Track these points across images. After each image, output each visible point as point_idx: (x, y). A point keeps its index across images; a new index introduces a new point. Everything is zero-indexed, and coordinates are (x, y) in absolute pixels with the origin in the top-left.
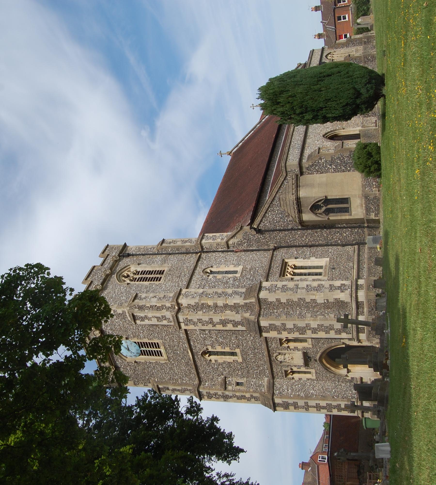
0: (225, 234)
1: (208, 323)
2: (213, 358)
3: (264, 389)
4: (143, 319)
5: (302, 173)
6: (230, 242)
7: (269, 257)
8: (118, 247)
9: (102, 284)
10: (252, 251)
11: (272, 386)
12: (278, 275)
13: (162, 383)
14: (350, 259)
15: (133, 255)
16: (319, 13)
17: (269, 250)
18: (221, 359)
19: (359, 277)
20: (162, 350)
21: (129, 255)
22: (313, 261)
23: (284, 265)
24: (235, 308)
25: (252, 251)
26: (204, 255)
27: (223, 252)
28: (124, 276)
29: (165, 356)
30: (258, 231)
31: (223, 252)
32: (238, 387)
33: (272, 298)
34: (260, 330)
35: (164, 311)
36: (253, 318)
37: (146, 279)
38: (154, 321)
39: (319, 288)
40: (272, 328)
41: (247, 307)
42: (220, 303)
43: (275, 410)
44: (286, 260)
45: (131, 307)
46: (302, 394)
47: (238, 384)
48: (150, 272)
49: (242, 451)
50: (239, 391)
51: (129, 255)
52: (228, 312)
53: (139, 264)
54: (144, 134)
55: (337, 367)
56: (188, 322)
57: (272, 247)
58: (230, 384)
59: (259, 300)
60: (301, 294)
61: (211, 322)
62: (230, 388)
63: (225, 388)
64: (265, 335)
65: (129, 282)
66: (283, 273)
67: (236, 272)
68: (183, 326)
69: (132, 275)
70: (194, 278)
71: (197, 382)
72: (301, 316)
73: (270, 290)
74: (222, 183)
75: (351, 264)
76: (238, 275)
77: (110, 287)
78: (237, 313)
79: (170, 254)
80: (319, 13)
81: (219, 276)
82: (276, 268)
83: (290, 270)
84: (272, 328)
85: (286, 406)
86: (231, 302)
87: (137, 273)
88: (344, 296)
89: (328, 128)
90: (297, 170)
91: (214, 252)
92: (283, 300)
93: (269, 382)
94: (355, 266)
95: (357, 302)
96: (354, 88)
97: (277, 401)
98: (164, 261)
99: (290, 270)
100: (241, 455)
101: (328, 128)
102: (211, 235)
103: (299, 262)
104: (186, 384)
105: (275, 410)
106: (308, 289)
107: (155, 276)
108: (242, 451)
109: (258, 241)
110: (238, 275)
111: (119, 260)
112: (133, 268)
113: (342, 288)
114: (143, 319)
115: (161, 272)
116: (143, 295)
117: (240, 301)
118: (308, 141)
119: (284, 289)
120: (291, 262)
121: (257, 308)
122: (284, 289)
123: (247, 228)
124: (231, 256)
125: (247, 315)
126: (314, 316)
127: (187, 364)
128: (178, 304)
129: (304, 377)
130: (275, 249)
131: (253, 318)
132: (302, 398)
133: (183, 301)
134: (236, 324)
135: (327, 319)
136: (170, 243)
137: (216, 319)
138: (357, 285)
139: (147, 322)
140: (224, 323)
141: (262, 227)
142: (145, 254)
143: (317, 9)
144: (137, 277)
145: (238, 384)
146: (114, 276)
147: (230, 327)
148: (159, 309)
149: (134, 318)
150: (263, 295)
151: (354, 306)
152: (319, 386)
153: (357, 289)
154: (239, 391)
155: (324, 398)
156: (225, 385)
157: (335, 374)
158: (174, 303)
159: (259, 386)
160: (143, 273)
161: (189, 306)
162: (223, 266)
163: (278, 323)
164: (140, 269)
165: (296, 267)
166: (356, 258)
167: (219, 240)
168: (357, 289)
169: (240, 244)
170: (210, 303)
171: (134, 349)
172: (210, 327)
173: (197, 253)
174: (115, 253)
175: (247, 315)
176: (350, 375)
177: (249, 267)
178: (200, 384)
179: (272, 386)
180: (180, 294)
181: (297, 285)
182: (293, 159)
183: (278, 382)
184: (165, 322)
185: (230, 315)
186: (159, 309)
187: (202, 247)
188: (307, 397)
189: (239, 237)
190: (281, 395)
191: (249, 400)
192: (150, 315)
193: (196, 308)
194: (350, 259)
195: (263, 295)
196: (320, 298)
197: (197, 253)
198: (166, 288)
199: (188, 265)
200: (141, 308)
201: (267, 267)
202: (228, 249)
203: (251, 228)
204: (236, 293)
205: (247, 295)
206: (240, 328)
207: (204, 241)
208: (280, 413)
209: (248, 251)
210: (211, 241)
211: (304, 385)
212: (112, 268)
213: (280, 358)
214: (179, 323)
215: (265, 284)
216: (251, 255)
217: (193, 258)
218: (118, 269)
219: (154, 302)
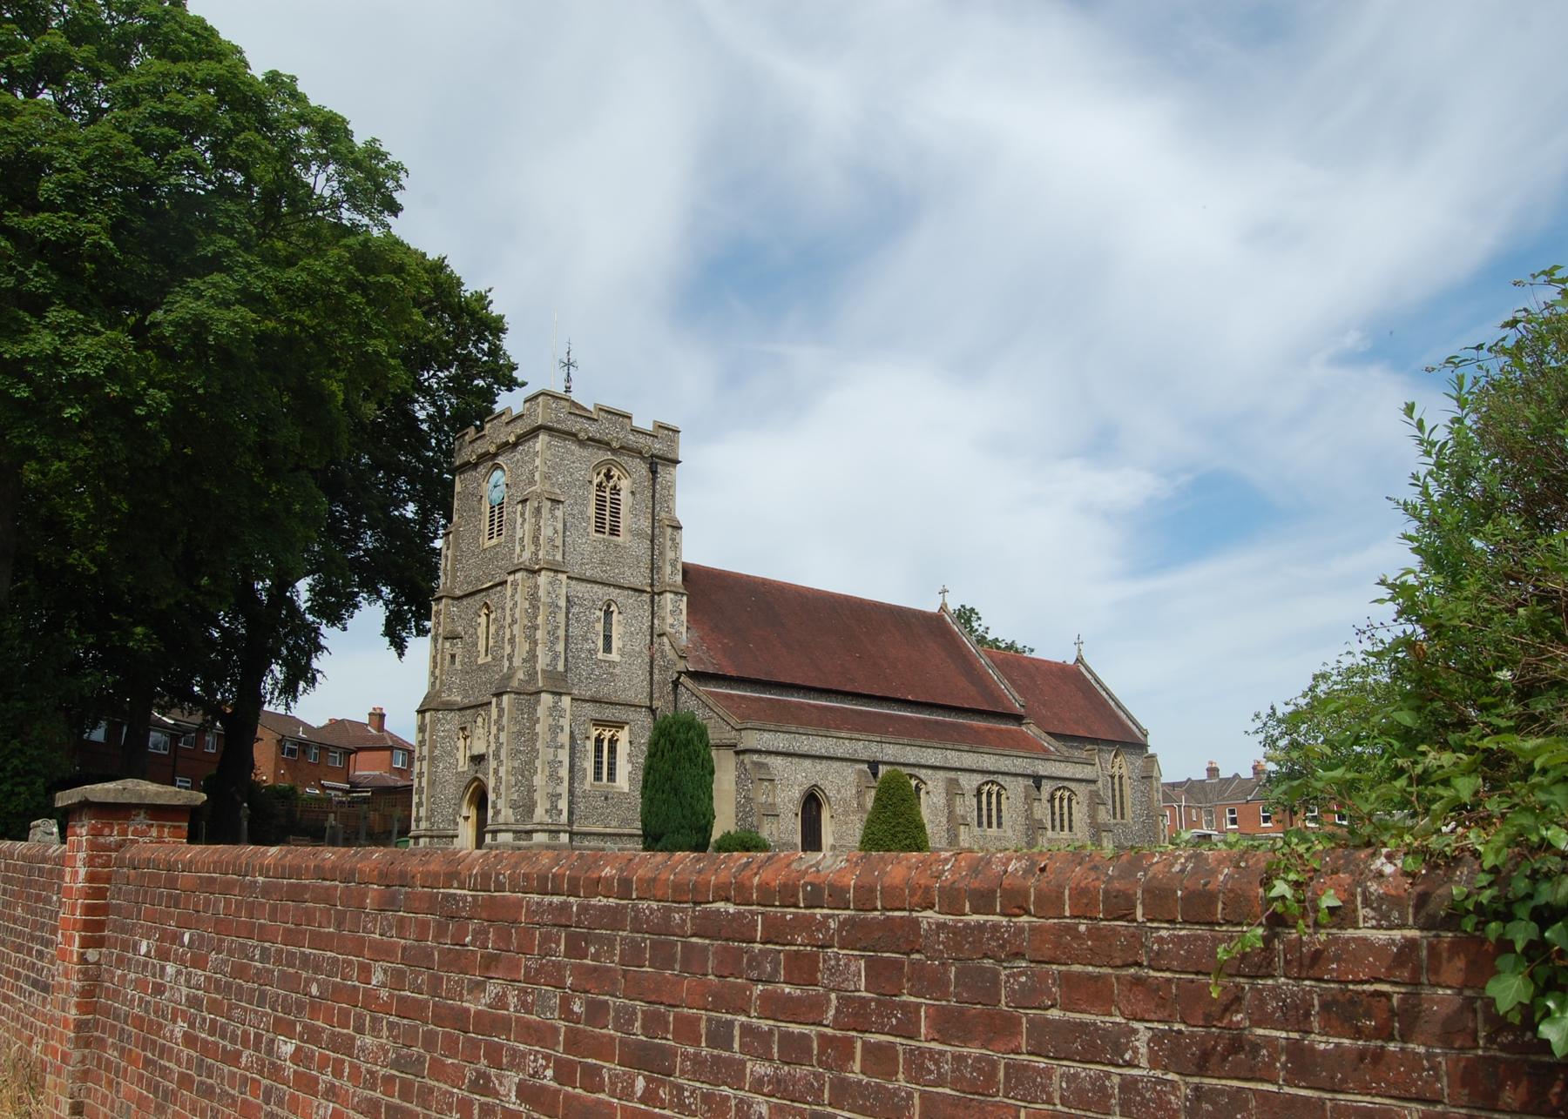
0: (684, 630)
1: (512, 616)
2: (483, 620)
3: (445, 697)
4: (522, 514)
5: (737, 753)
6: (665, 639)
7: (636, 702)
8: (674, 449)
9: (589, 439)
10: (651, 674)
11: (449, 707)
12: (597, 716)
13: (456, 539)
14: (625, 822)
15: (654, 479)
16: (1203, 776)
17: (651, 700)
18: (482, 631)
19: (515, 832)
20: (494, 541)
21: (654, 472)
22: (623, 768)
23: (619, 725)
24: (532, 657)
25: (651, 674)
26: (646, 597)
27: (652, 627)
28: (609, 471)
29: (488, 544)
30: (676, 684)
31: (652, 627)
32: (448, 657)
33: (541, 711)
34: (499, 695)
35: (533, 548)
36: (515, 683)
37: (600, 507)
38: (519, 534)
39: (554, 777)
40: (501, 710)
41: (532, 675)
42: (539, 634)
43: (419, 712)
44: (627, 728)
45: (539, 495)
46: (437, 752)
47: (453, 656)
48: (615, 513)
49: (401, 655)
50: (443, 659)
51: (654, 472)
52: (527, 647)
53: (633, 493)
54: (1351, 340)
55: (471, 802)
56: (515, 584)
57: (656, 704)
58: (453, 645)
59: (539, 693)
60: (545, 754)
61: (514, 622)
62: (447, 645)
63: (446, 638)
64: (494, 700)
65: (596, 482)
66: (598, 723)
67: (608, 648)
68: (510, 578)
69: (611, 484)
70: (596, 587)
71: (458, 593)
72: (514, 754)
73: (555, 707)
74: (862, 600)
75: (614, 824)
76: (600, 655)
77: (585, 453)
78: (524, 660)
79: (652, 541)
80: (1203, 776)
81: (599, 627)
82: (608, 713)
83: (607, 734)
84: (501, 710)
85: (422, 729)
86: (540, 650)
87: (616, 490)
88: (540, 813)
89: (839, 792)
90: (741, 747)
91: (653, 613)
92: (538, 728)
93: (455, 703)
94: (608, 830)
95: (532, 832)
96: (662, 835)
97: (428, 715)
98: (637, 534)
99: (607, 734)
100: (393, 652)
101: (839, 792)
102: (684, 606)
103: (623, 748)
104: (454, 577)
105: (419, 712)
106: (554, 764)
107: (608, 521)
108: (401, 655)
109: (665, 683)
110: (600, 655)
111: (643, 458)
112: (625, 484)
113: (553, 810)
114: (522, 514)
115: (614, 531)
116: (559, 513)
117: (542, 662)
118: (807, 763)
119: (555, 729)
120: (623, 736)
121: (532, 689)
122: (555, 729)
123: (681, 666)
124: (641, 643)
125: (520, 675)
126: (513, 771)
127: (478, 579)
128: (540, 570)
129: (460, 755)
130: (652, 710)
131: (515, 683)
132: (431, 751)
133: (543, 578)
134: (510, 658)
135: (508, 788)
136: (673, 540)
137: (516, 628)
138: (559, 832)
139: (519, 521)
140: (512, 641)
141: (682, 689)
142: (657, 499)
143: (1213, 771)
144: (607, 494)
145: (453, 656)
146: (609, 456)
147: (508, 649)
148: (536, 540)
149: (524, 501)
150: (546, 699)
151: (529, 827)
152: (449, 776)
153: (551, 832)
154: (443, 659)
155: (432, 783)
156: (452, 637)
157: (462, 799)
158: (542, 564)
159: (450, 689)
160: (616, 502)
161: (537, 587)
162: (621, 630)
163: (505, 720)
164: (624, 496)
165: (613, 743)
166: (626, 831)
167: (670, 620)
168: (551, 832)
169: (663, 656)
170: (540, 620)
171: (496, 496)
172: (509, 620)
173: (652, 585)
174: (658, 447)
175: (520, 675)
176: (460, 820)
177: (617, 671)
178: (453, 598)
179: (449, 707)
180: (556, 571)
181: (562, 746)
182: (752, 739)
183: (454, 718)
184: (518, 549)
185: (523, 648)
186: (536, 540)
187: (660, 594)
188: (433, 759)
189: (671, 654)
190: (434, 722)
191: (433, 673)
192: (526, 526)
193: (533, 598)
194: (625, 822)
195: (546, 699)
196: (539, 780)
197: (652, 585)
198: (587, 540)
199: (628, 573)
200: (538, 510)
201: (614, 699)
202: (654, 634)
203: (680, 673)
204: (556, 657)
205: (550, 674)
206: (506, 664)
207: (669, 596)
208: (414, 719)
209: (651, 667)
210: (669, 607)
211: (450, 754)
212: (624, 449)
213: (480, 720)
214: (514, 572)
215: (566, 700)
216: (641, 677)
217: (641, 581)
218: (623, 459)
219: (546, 531)
